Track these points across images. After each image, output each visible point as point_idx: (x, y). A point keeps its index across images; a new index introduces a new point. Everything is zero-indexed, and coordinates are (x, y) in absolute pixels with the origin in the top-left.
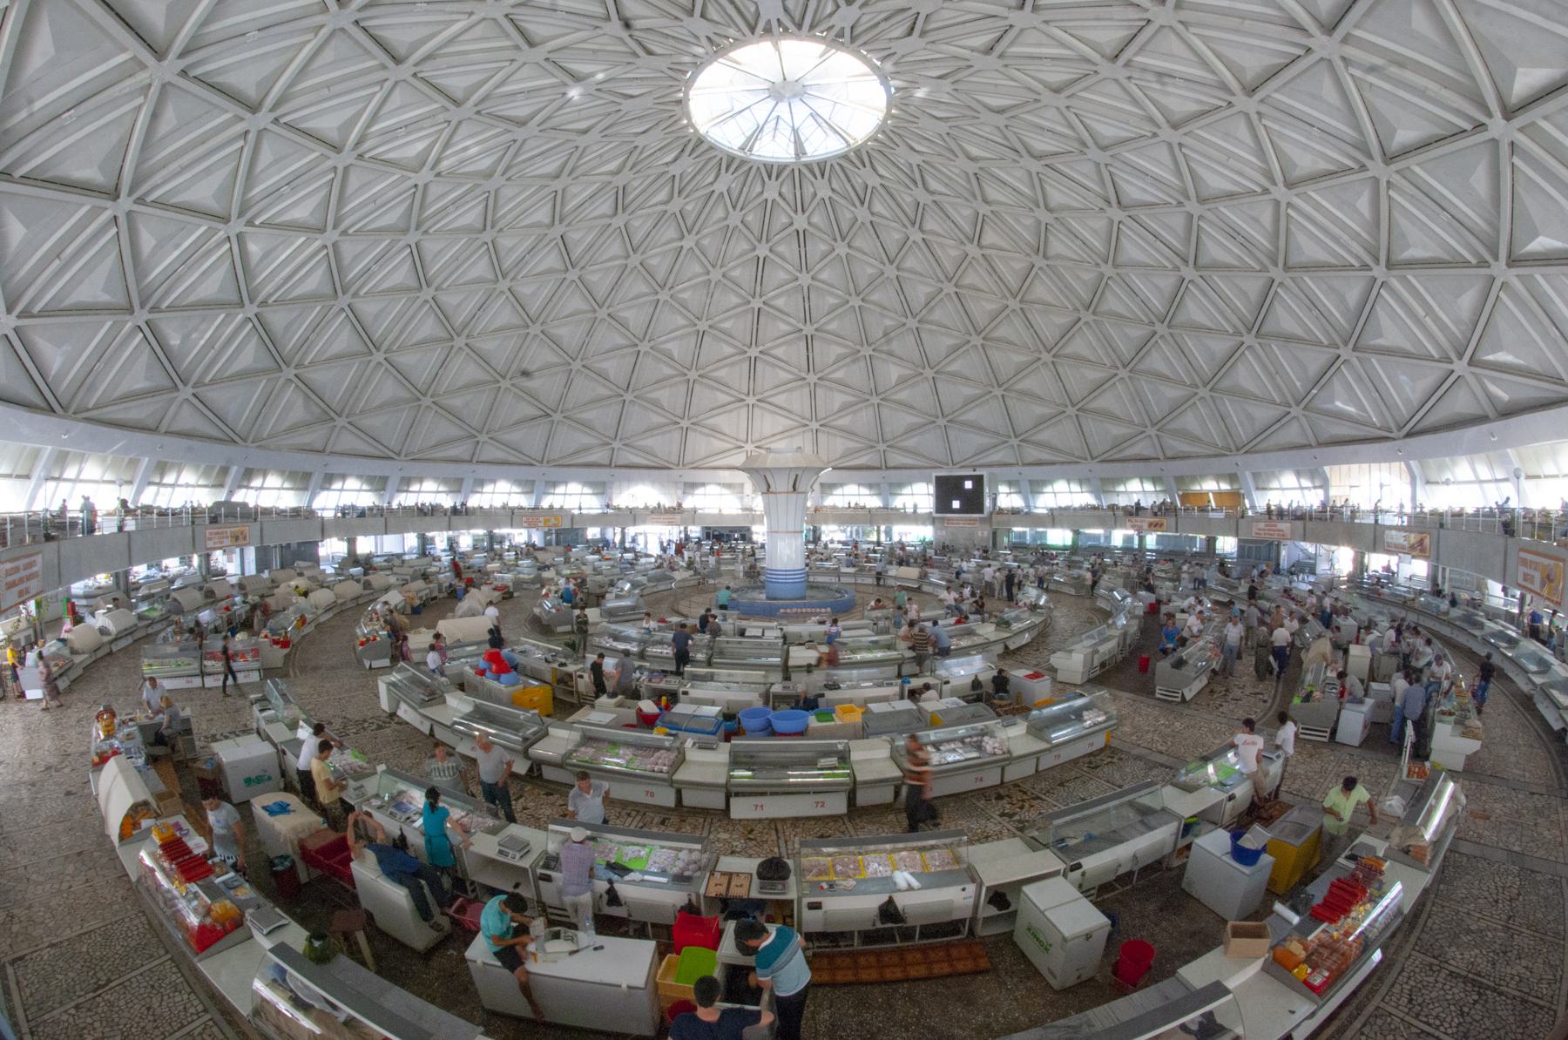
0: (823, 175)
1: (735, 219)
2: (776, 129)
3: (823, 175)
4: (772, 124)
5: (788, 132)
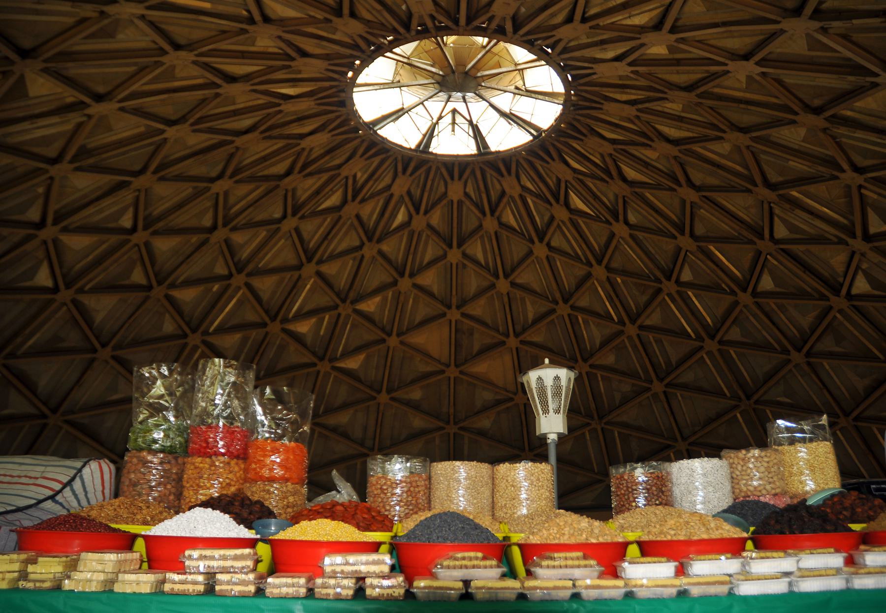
0: (509, 172)
1: (419, 223)
2: (454, 123)
3: (509, 172)
4: (448, 119)
5: (466, 126)
